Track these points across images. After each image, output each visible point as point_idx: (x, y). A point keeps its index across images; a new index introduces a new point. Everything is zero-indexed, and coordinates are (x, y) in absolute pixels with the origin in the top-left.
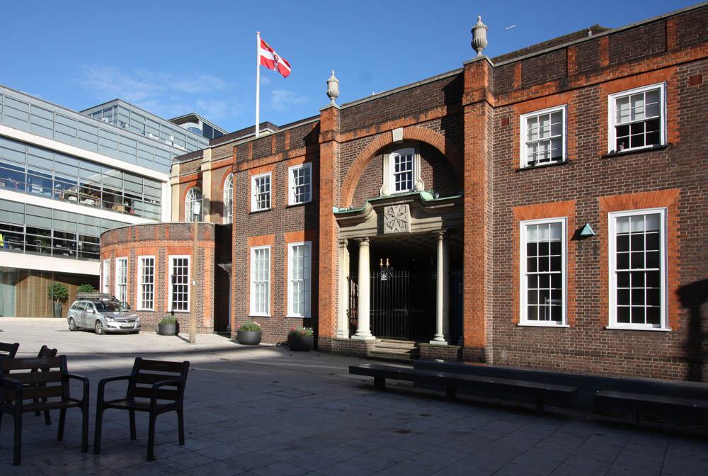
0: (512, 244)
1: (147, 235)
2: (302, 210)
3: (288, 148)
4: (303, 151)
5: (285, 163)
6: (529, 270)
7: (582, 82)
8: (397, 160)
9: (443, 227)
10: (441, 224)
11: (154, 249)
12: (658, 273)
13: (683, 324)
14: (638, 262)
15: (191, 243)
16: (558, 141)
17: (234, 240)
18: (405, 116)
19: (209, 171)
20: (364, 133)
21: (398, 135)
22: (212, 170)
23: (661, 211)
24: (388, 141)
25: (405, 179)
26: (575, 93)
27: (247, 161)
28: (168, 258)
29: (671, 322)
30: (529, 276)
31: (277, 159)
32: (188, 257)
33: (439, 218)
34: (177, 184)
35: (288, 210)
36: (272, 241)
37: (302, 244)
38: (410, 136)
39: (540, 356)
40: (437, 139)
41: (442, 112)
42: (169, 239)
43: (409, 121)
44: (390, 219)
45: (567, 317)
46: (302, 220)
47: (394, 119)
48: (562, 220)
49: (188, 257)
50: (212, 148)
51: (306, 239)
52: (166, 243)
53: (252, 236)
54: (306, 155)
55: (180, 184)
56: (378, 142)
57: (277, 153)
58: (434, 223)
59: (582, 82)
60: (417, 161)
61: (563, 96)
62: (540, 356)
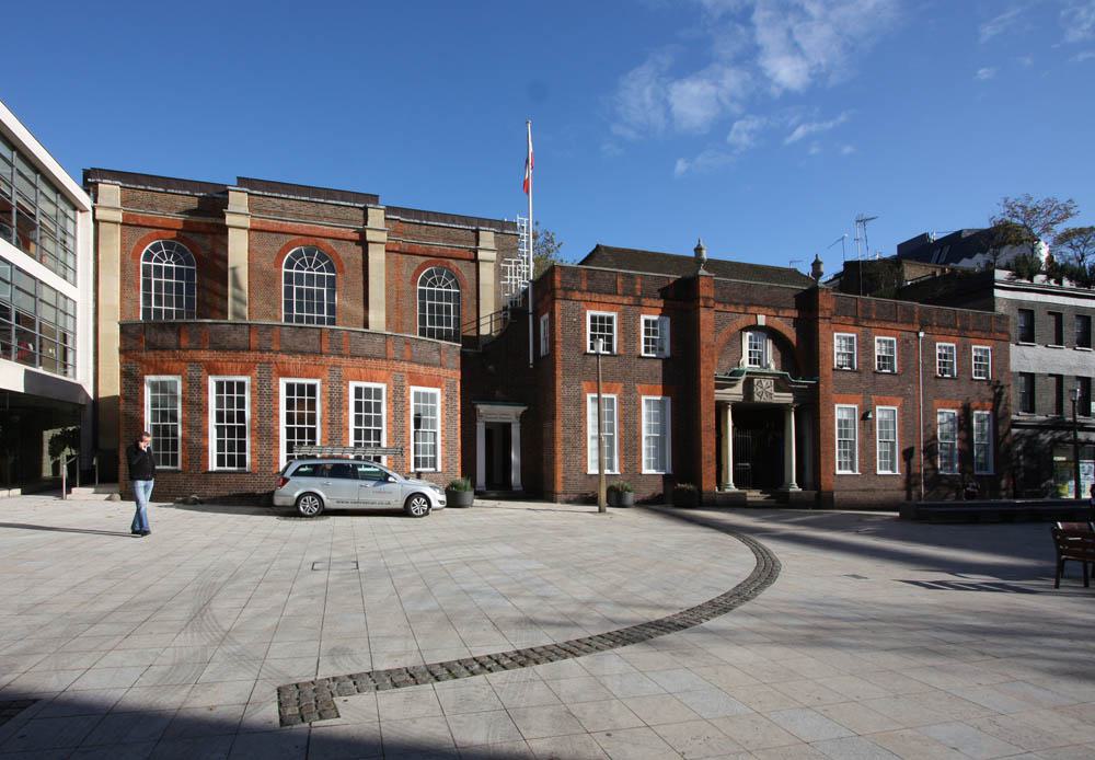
0: (342, 396)
1: (368, 349)
2: (659, 364)
3: (639, 293)
4: (661, 303)
5: (637, 308)
6: (217, 421)
7: (864, 324)
8: (750, 338)
9: (794, 402)
10: (792, 399)
11: (383, 374)
12: (315, 429)
13: (905, 469)
14: (301, 421)
15: (442, 371)
16: (851, 356)
17: (559, 382)
18: (768, 307)
19: (246, 231)
20: (732, 309)
21: (762, 320)
22: (251, 230)
23: (856, 407)
24: (753, 323)
25: (302, 298)
26: (861, 329)
27: (581, 291)
28: (409, 390)
29: (900, 470)
30: (287, 428)
31: (625, 301)
32: (317, 382)
33: (791, 395)
34: (116, 223)
35: (641, 361)
36: (619, 390)
37: (659, 398)
38: (771, 325)
39: (847, 494)
40: (791, 334)
41: (795, 314)
42: (411, 361)
43: (771, 312)
44: (760, 390)
45: (859, 468)
46: (660, 373)
47: (758, 305)
48: (856, 407)
49: (317, 382)
50: (249, 194)
51: (664, 394)
52: (406, 366)
53: (589, 381)
54: (663, 309)
55: (123, 224)
56: (743, 321)
57: (624, 295)
58: (786, 398)
59: (864, 324)
60: (770, 344)
61: (855, 328)
62: (847, 494)
